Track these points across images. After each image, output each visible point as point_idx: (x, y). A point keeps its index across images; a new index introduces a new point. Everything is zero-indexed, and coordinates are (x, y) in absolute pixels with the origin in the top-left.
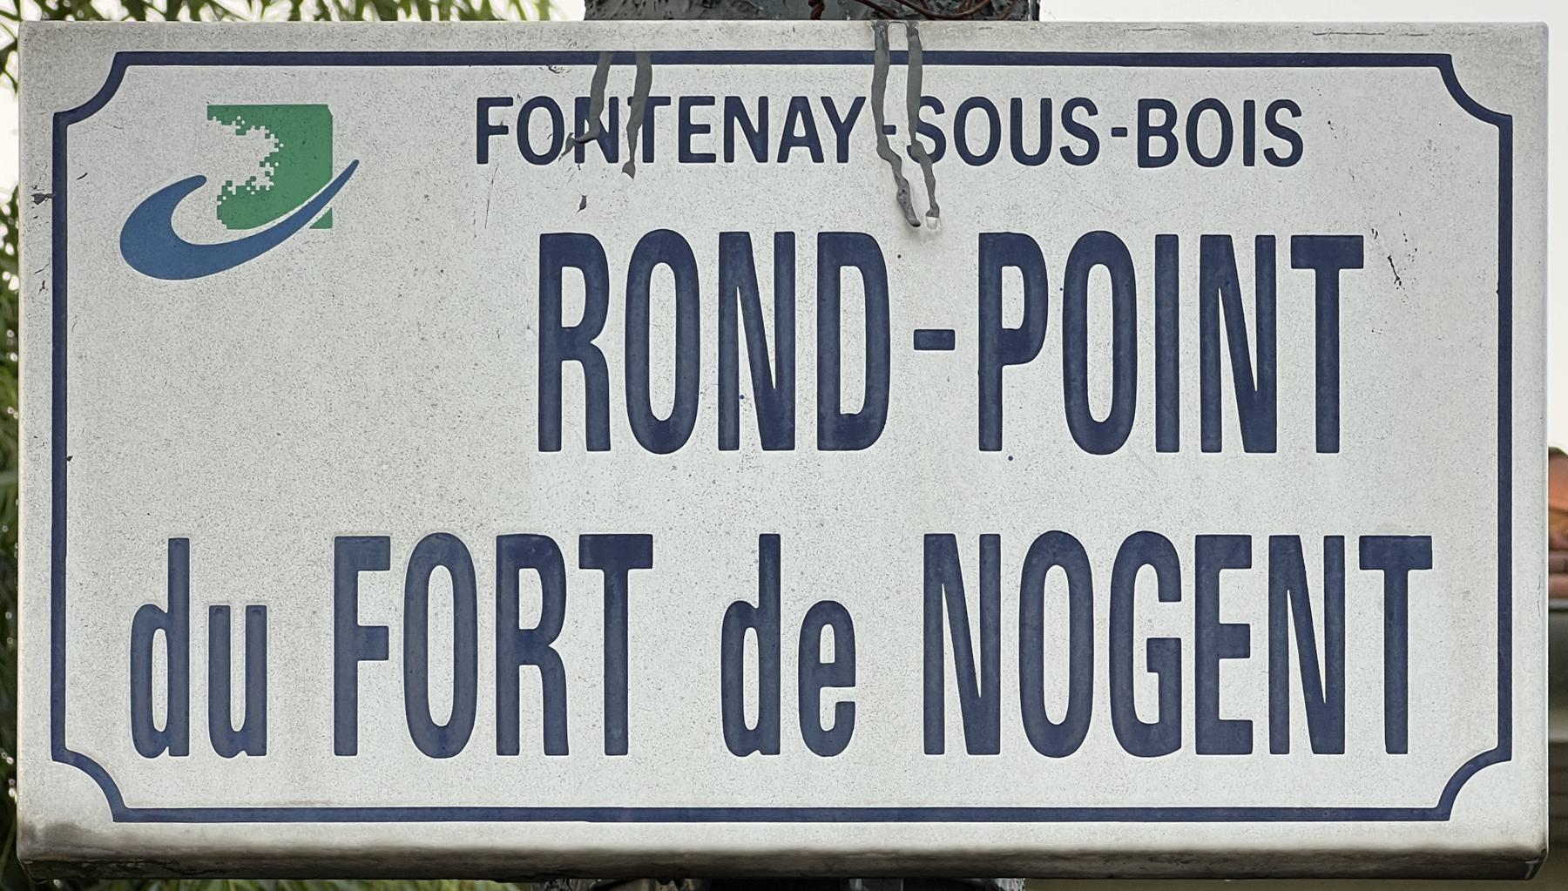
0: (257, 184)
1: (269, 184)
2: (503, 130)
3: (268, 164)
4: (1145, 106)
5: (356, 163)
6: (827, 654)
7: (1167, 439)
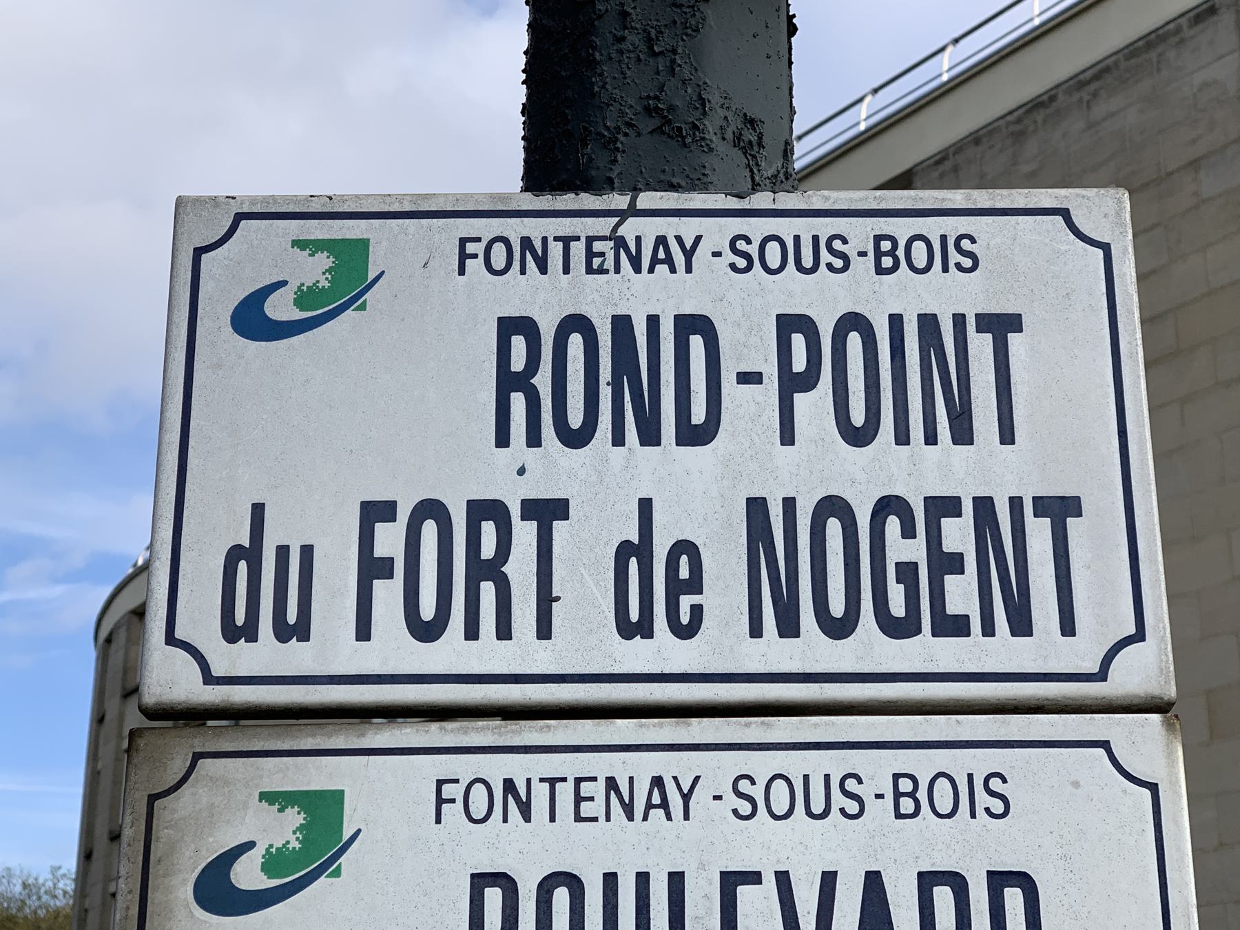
0: (290, 846)
1: (327, 285)
2: (475, 256)
3: (298, 833)
4: (878, 239)
5: (359, 831)
6: (684, 573)
7: (902, 437)
